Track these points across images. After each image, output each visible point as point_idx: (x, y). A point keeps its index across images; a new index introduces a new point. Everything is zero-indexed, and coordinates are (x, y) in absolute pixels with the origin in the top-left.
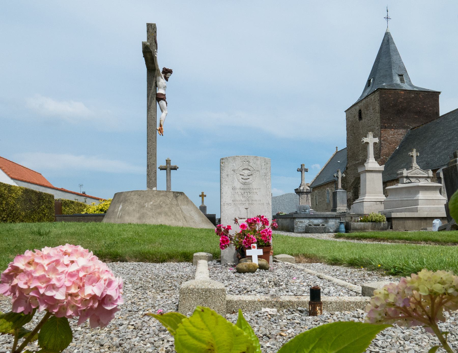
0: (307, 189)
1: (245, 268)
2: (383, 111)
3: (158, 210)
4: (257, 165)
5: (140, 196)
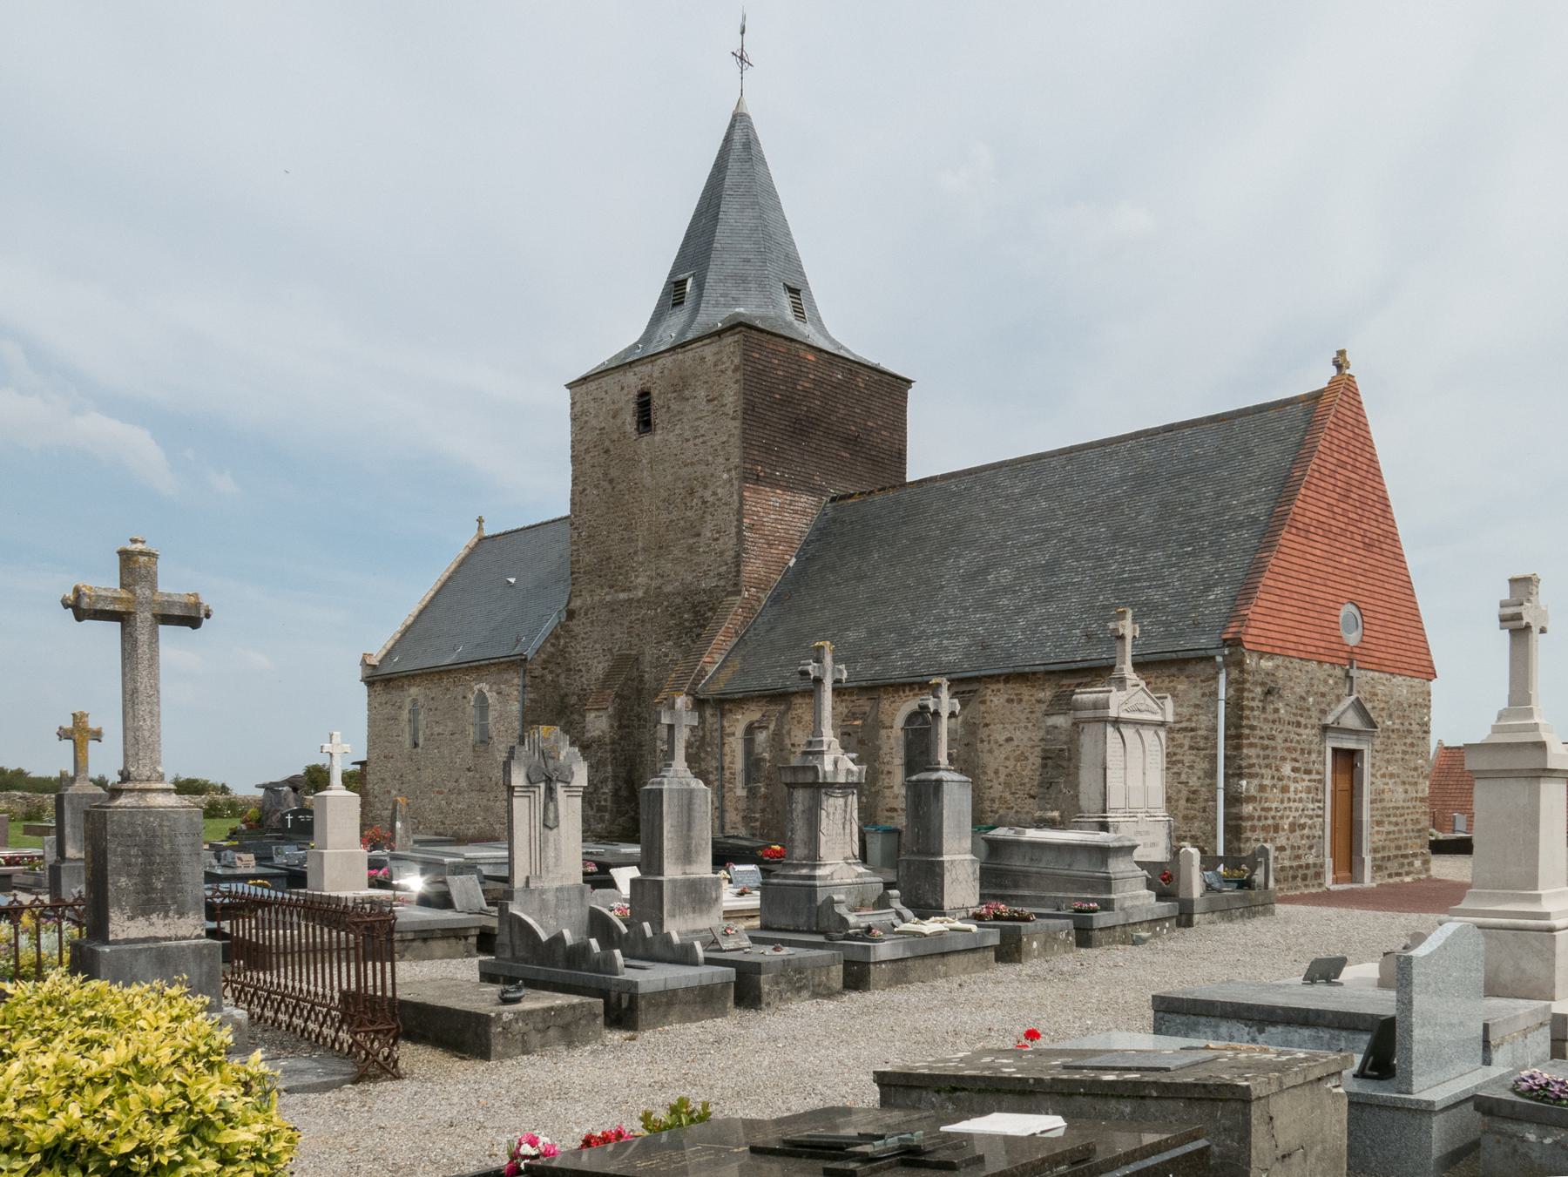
0: (849, 771)
2: (751, 412)
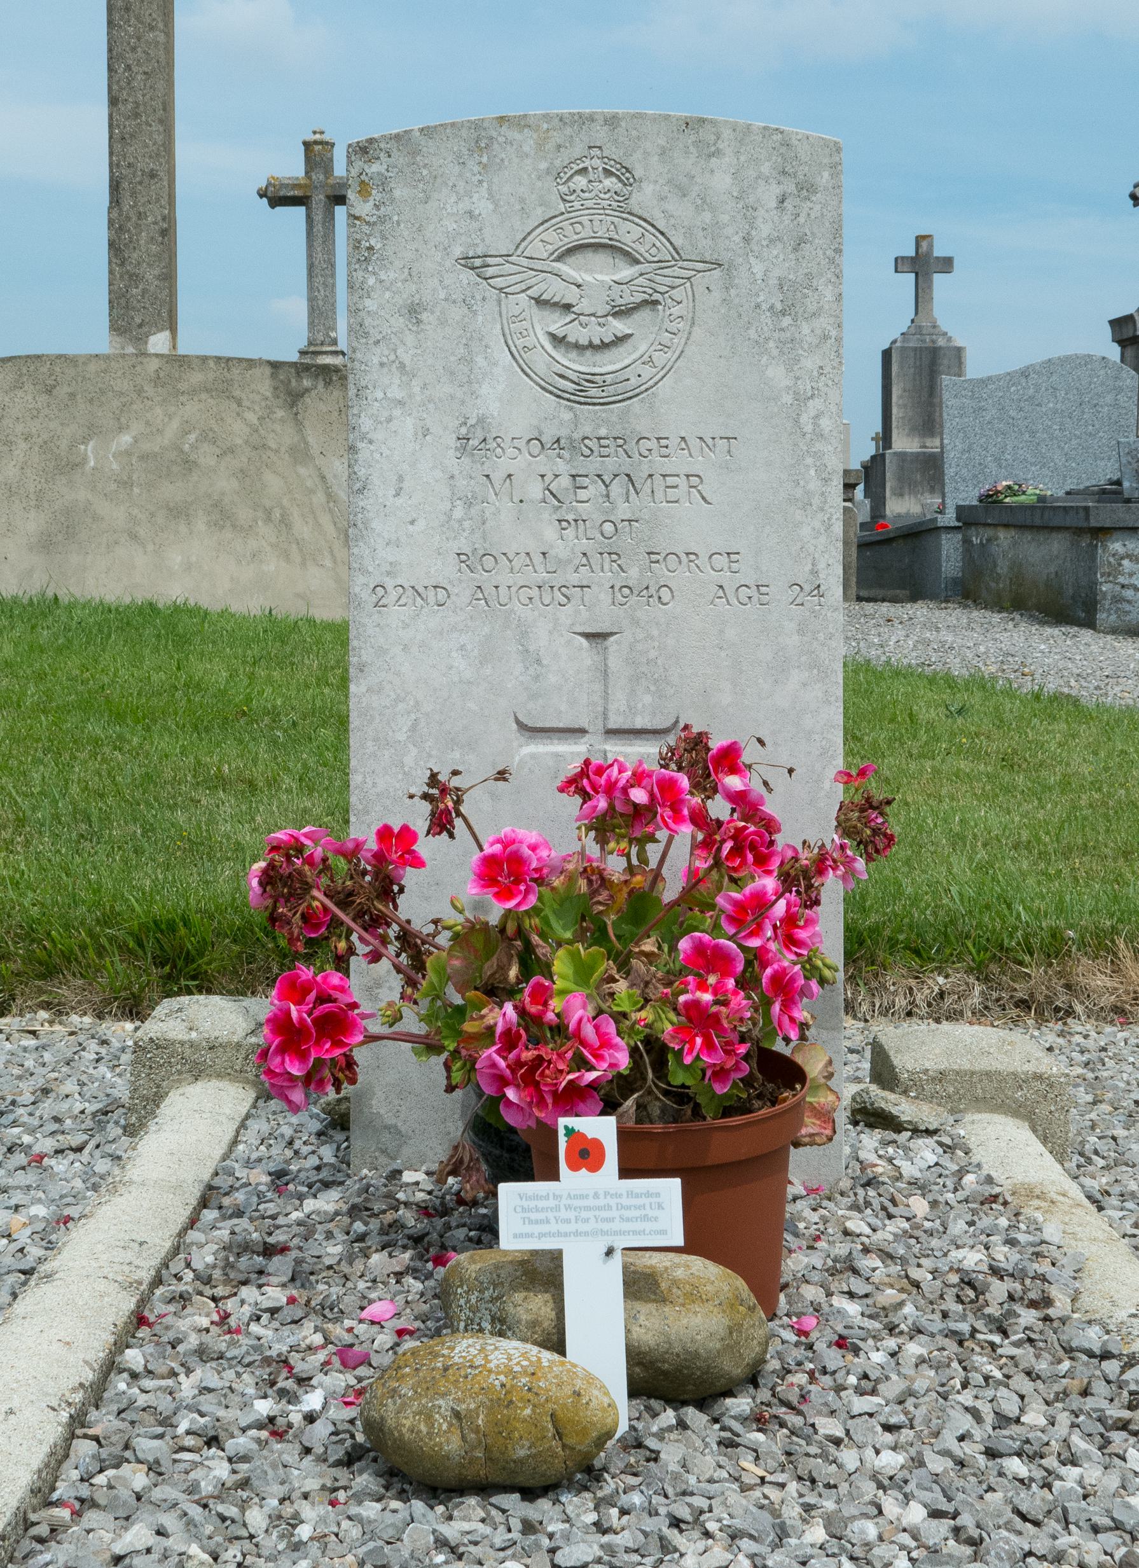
1: (453, 1445)
3: (172, 491)
4: (704, 203)
5: (49, 391)
